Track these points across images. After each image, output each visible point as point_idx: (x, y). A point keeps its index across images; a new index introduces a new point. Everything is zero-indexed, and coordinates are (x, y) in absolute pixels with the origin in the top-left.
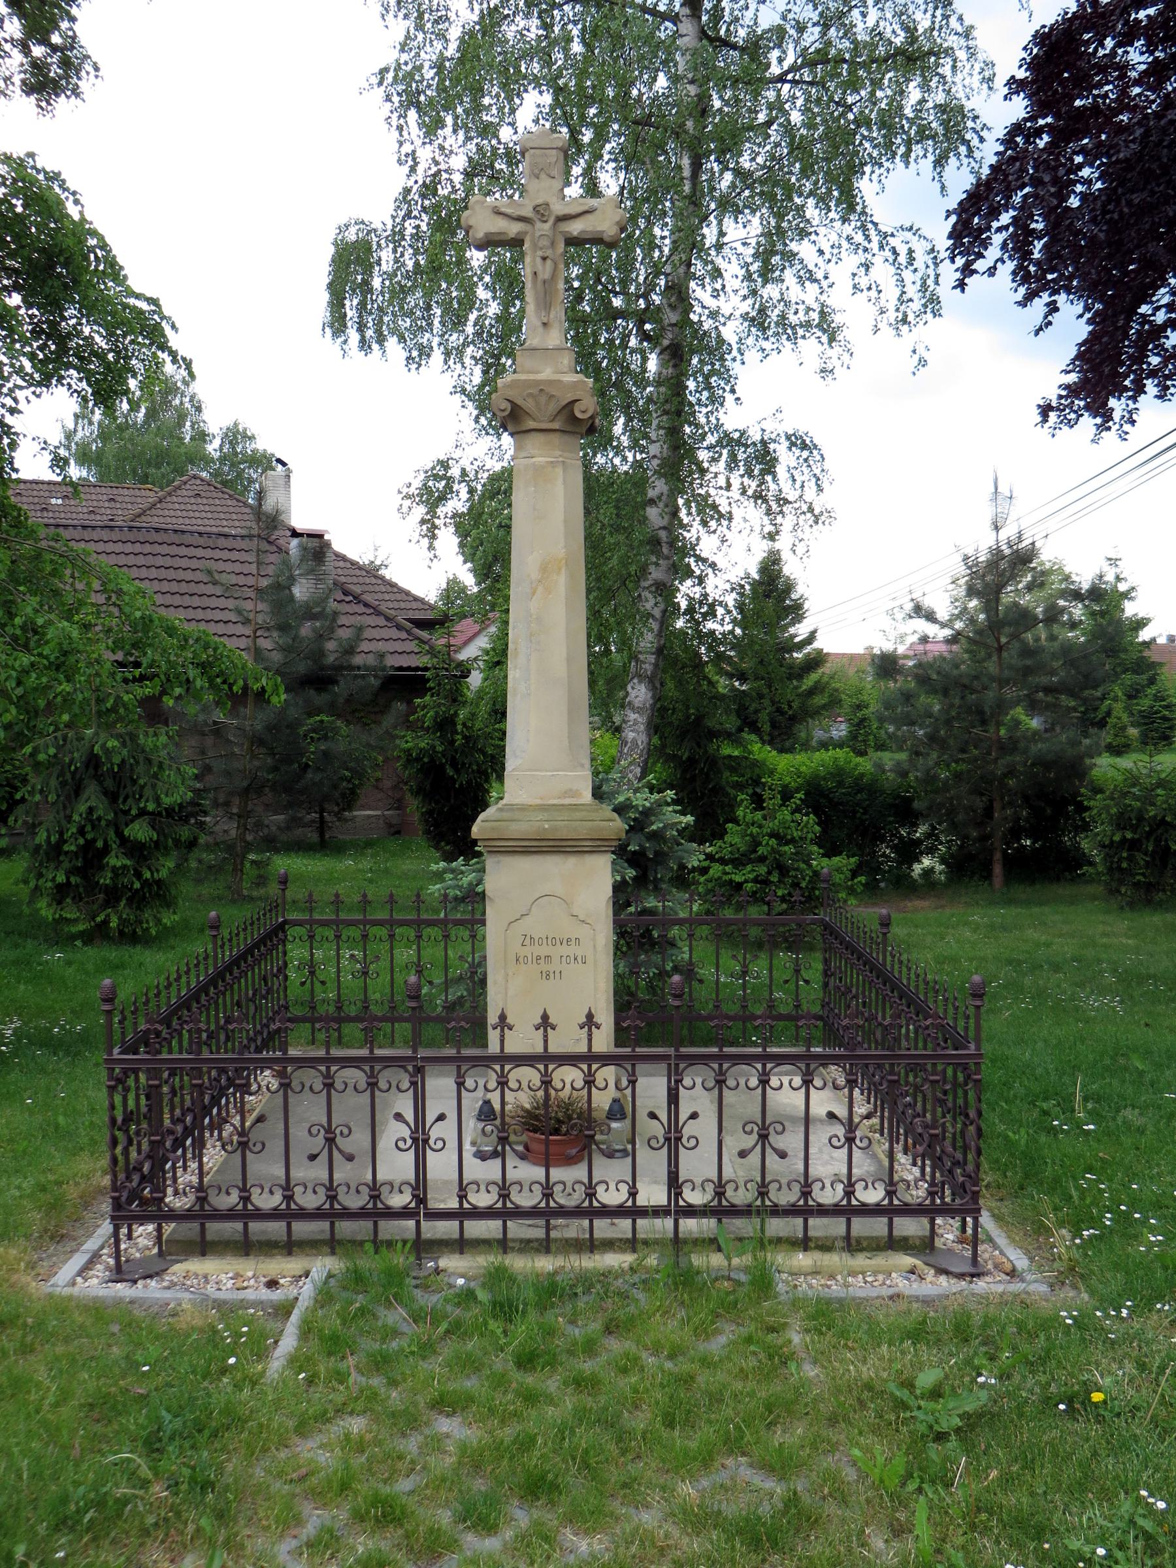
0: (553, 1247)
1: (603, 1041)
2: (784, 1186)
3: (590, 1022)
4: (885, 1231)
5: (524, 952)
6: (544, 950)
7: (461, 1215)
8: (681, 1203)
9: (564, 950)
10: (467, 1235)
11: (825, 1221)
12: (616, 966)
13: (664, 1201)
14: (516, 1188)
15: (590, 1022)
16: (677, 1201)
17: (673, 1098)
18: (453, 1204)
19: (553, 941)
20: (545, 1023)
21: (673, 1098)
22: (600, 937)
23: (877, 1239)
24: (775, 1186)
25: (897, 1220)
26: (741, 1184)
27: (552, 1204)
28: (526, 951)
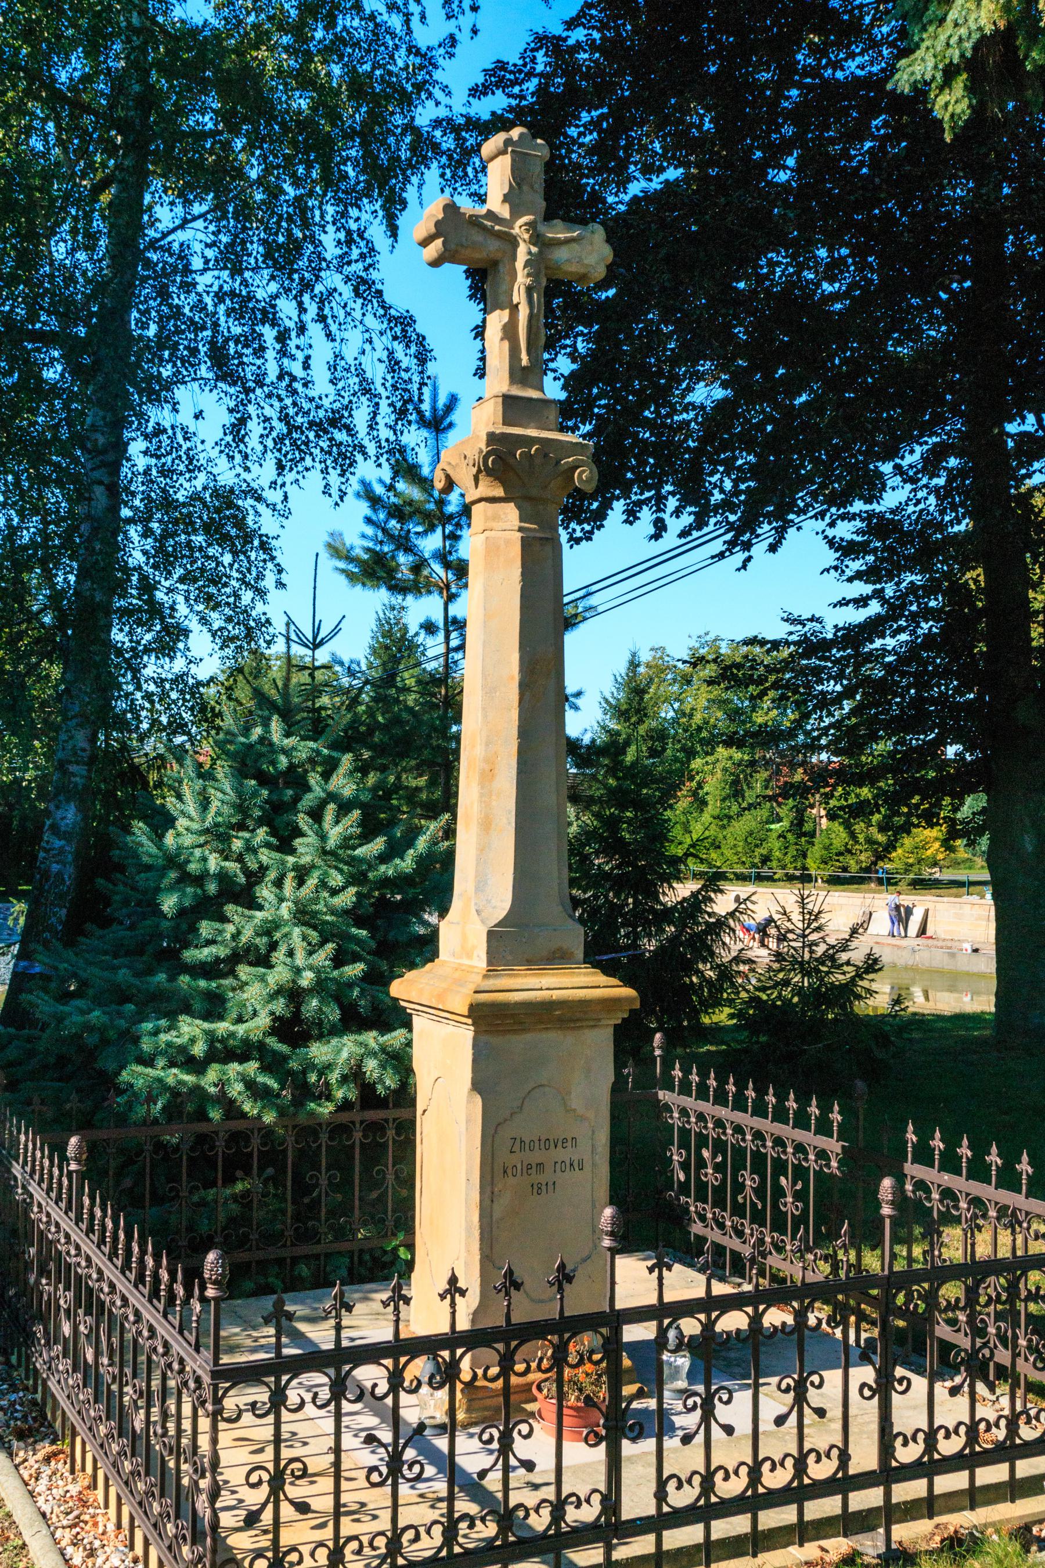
0: (979, 1498)
6: (536, 1157)
28: (515, 1159)
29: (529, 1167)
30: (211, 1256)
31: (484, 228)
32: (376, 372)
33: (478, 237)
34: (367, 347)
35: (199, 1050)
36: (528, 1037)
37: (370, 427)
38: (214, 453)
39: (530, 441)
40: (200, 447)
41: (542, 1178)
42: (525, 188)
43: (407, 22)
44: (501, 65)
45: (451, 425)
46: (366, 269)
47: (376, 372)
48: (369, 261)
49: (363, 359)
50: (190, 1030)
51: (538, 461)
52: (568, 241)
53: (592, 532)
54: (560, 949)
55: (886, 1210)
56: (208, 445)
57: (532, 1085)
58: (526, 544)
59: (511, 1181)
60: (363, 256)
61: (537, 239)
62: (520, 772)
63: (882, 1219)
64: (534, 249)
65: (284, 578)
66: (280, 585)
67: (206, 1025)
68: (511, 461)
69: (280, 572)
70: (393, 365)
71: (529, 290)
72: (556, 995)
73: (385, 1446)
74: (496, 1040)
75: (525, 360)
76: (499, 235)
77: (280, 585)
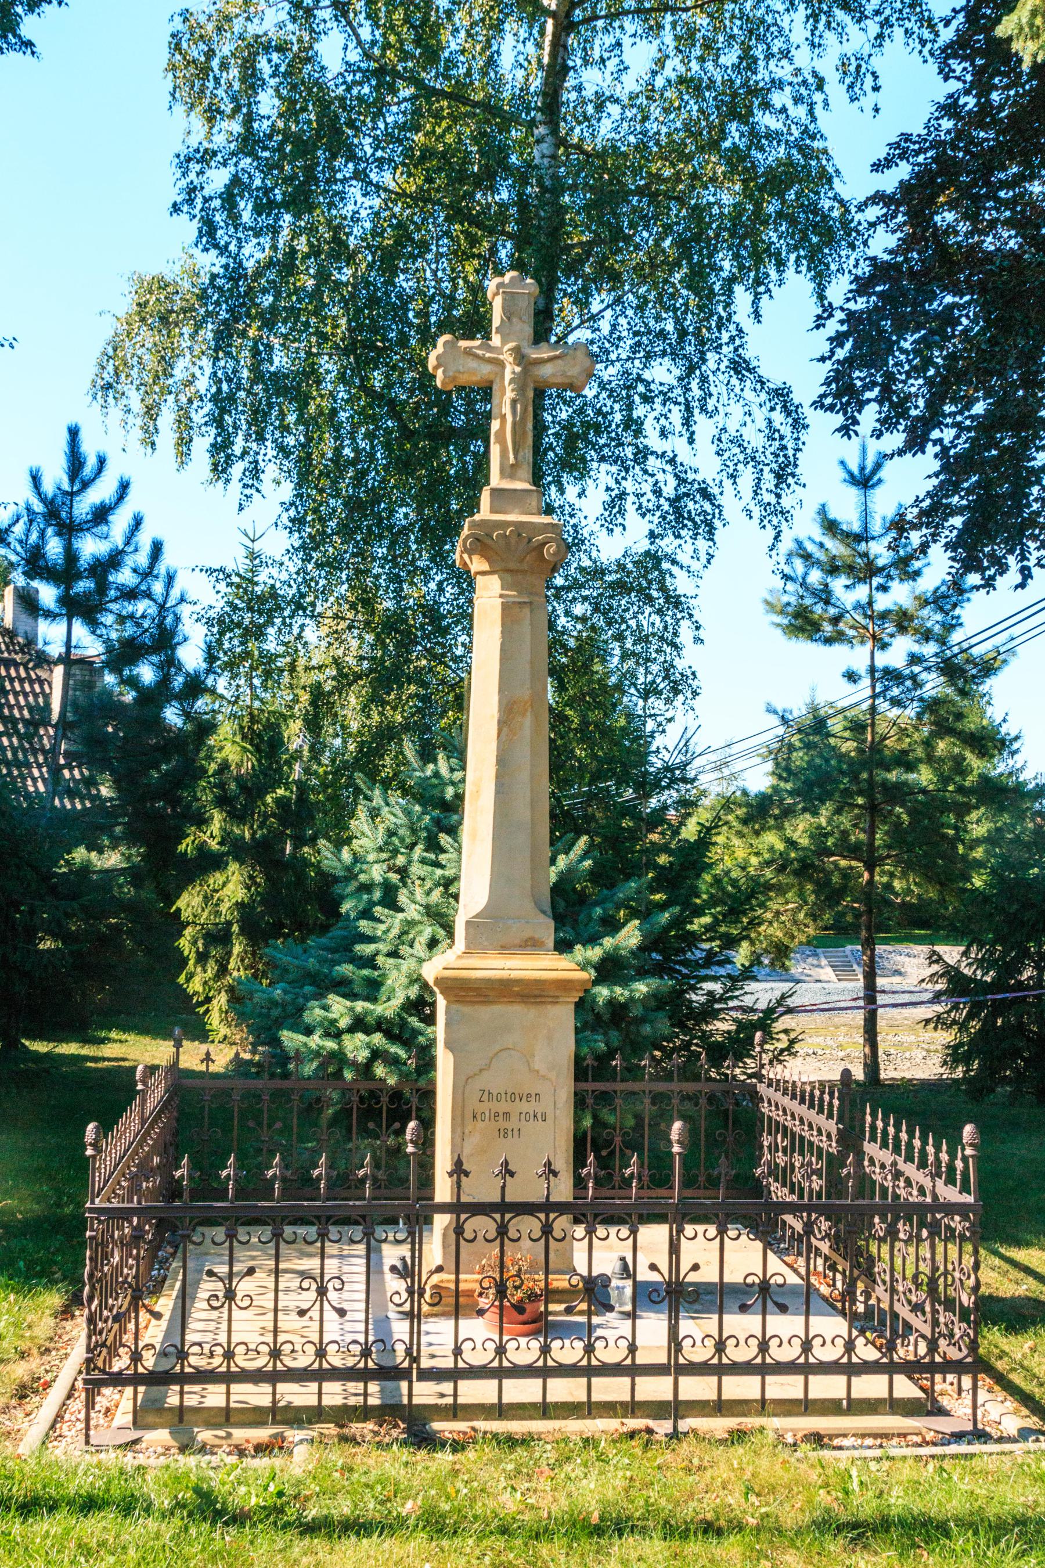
0: (770, 1408)
1: (563, 1190)
2: (742, 1342)
3: (551, 1171)
4: (842, 1394)
5: (481, 1108)
6: (503, 1107)
7: (453, 1375)
8: (681, 1361)
9: (525, 1107)
10: (506, 1400)
11: (249, 1387)
12: (577, 1121)
13: (664, 1360)
14: (776, 1341)
15: (551, 1171)
16: (676, 1358)
17: (674, 1249)
18: (448, 1363)
19: (513, 1097)
20: (507, 1171)
21: (674, 1249)
22: (560, 1093)
23: (258, 1409)
24: (776, 1341)
25: (551, 1382)
26: (785, 1341)
27: (279, 1365)
28: (485, 1107)
29: (497, 1114)
30: (91, 1126)
31: (476, 356)
32: (755, 439)
33: (472, 364)
34: (747, 418)
35: (344, 1023)
36: (497, 1009)
37: (756, 493)
38: (596, 527)
39: (506, 524)
40: (584, 522)
41: (509, 1125)
42: (515, 320)
43: (811, 112)
44: (906, 137)
45: (880, 481)
46: (736, 349)
47: (755, 439)
48: (738, 342)
49: (744, 431)
50: (339, 1008)
51: (513, 540)
52: (551, 359)
53: (992, 578)
54: (532, 938)
55: (676, 1149)
56: (591, 519)
57: (498, 1048)
58: (506, 608)
59: (480, 1125)
60: (732, 339)
61: (520, 357)
62: (497, 792)
63: (671, 1155)
64: (518, 369)
65: (702, 634)
66: (698, 640)
67: (348, 1004)
68: (488, 541)
69: (698, 628)
70: (772, 433)
71: (514, 402)
72: (515, 975)
73: (221, 1280)
74: (467, 1009)
75: (512, 460)
76: (490, 361)
77: (698, 640)
